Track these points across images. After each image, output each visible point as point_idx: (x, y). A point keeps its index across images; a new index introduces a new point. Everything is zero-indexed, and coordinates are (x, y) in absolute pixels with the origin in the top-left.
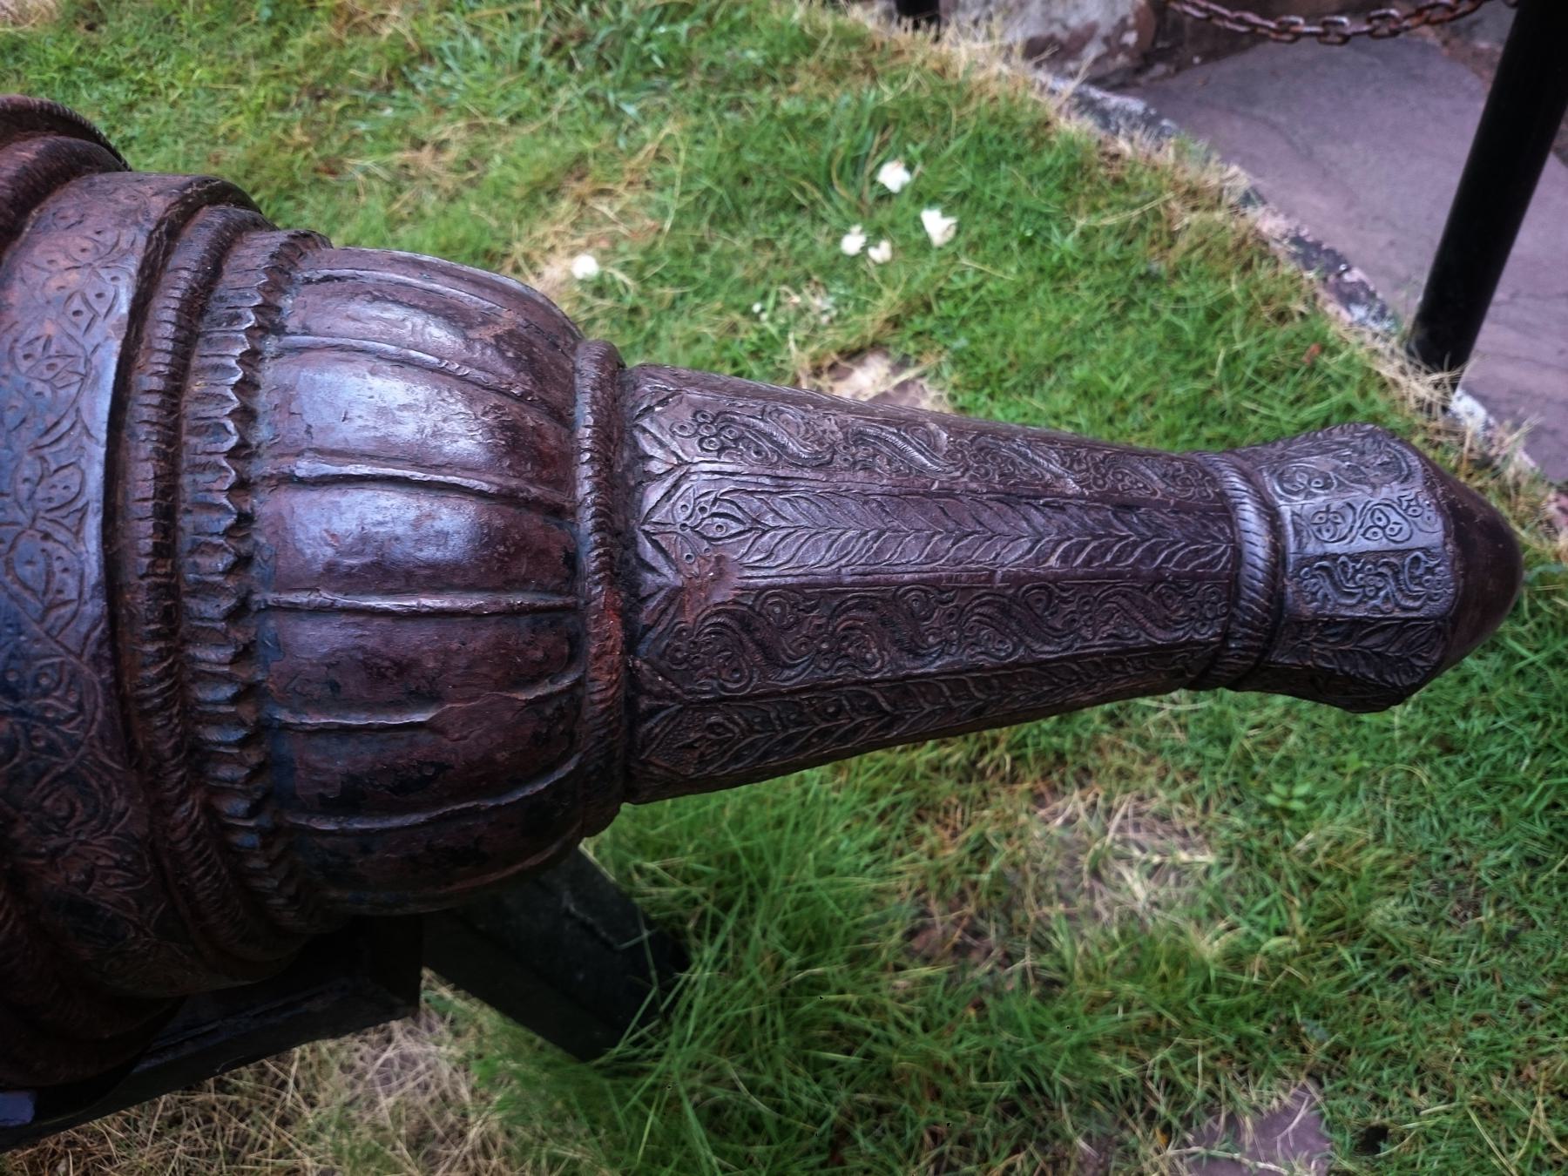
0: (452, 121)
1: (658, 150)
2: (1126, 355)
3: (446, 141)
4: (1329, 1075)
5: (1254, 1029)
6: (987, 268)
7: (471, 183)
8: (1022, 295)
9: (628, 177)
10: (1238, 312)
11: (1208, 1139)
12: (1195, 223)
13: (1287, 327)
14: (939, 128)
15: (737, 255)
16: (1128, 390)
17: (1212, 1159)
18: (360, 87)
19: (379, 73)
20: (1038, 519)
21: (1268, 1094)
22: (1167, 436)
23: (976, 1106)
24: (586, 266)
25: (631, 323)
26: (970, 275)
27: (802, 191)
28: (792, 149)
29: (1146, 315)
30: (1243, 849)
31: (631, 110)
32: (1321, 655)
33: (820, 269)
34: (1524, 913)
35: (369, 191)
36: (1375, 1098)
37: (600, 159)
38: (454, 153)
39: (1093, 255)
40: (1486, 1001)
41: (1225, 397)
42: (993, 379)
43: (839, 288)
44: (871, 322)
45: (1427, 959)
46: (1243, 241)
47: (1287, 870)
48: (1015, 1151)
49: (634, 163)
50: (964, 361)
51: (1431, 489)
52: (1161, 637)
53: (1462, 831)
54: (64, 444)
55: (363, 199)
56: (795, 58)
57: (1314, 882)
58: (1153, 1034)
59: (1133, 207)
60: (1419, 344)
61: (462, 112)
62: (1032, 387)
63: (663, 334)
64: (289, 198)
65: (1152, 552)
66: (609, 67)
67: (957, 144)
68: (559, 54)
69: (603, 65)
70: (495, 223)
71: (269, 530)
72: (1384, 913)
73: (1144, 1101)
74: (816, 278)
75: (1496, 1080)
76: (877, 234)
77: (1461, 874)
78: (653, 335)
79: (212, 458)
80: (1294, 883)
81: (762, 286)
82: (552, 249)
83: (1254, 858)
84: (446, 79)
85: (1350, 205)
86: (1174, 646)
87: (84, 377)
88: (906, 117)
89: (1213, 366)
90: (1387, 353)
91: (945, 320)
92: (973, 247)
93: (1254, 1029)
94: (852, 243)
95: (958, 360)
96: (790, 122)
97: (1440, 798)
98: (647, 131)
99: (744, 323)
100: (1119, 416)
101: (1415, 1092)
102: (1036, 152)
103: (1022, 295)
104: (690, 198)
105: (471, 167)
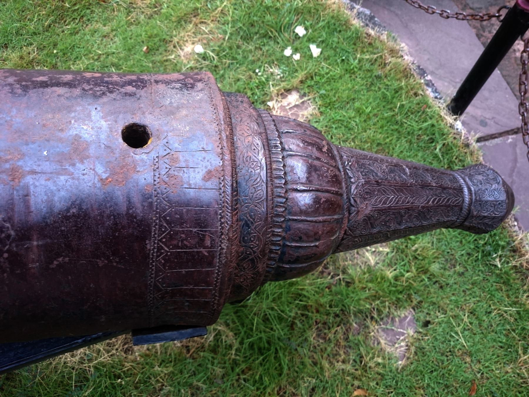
1: (222, 10)
2: (370, 101)
4: (417, 308)
5: (400, 296)
6: (330, 67)
8: (341, 77)
9: (212, 18)
10: (403, 91)
11: (386, 324)
12: (394, 62)
13: (417, 98)
14: (316, 17)
15: (251, 51)
16: (370, 112)
17: (387, 329)
20: (427, 192)
21: (403, 313)
22: (381, 128)
23: (328, 314)
24: (199, 49)
25: (215, 71)
26: (325, 69)
27: (271, 32)
28: (268, 17)
29: (377, 89)
30: (397, 248)
32: (475, 223)
33: (277, 60)
34: (465, 267)
35: (119, 11)
36: (427, 314)
37: (202, 11)
39: (362, 66)
40: (455, 290)
41: (399, 118)
42: (331, 104)
44: (295, 81)
45: (442, 279)
46: (406, 69)
47: (410, 255)
48: (338, 326)
49: (214, 14)
50: (323, 97)
51: (504, 186)
52: (446, 219)
53: (453, 246)
54: (259, 184)
55: (116, 13)
57: (416, 258)
58: (376, 297)
59: (375, 54)
60: (452, 107)
62: (342, 108)
63: (226, 76)
65: (448, 200)
70: (166, 29)
72: (435, 268)
73: (370, 314)
74: (276, 62)
75: (456, 309)
77: (452, 257)
78: (223, 76)
80: (411, 258)
81: (260, 64)
82: (187, 41)
83: (400, 251)
85: (418, 45)
86: (448, 221)
87: (260, 167)
88: (305, 11)
89: (396, 107)
90: (442, 108)
91: (317, 83)
92: (326, 59)
93: (400, 296)
94: (288, 52)
95: (322, 97)
97: (448, 237)
99: (253, 75)
100: (368, 120)
101: (437, 312)
102: (346, 31)
103: (341, 77)
104: (234, 29)
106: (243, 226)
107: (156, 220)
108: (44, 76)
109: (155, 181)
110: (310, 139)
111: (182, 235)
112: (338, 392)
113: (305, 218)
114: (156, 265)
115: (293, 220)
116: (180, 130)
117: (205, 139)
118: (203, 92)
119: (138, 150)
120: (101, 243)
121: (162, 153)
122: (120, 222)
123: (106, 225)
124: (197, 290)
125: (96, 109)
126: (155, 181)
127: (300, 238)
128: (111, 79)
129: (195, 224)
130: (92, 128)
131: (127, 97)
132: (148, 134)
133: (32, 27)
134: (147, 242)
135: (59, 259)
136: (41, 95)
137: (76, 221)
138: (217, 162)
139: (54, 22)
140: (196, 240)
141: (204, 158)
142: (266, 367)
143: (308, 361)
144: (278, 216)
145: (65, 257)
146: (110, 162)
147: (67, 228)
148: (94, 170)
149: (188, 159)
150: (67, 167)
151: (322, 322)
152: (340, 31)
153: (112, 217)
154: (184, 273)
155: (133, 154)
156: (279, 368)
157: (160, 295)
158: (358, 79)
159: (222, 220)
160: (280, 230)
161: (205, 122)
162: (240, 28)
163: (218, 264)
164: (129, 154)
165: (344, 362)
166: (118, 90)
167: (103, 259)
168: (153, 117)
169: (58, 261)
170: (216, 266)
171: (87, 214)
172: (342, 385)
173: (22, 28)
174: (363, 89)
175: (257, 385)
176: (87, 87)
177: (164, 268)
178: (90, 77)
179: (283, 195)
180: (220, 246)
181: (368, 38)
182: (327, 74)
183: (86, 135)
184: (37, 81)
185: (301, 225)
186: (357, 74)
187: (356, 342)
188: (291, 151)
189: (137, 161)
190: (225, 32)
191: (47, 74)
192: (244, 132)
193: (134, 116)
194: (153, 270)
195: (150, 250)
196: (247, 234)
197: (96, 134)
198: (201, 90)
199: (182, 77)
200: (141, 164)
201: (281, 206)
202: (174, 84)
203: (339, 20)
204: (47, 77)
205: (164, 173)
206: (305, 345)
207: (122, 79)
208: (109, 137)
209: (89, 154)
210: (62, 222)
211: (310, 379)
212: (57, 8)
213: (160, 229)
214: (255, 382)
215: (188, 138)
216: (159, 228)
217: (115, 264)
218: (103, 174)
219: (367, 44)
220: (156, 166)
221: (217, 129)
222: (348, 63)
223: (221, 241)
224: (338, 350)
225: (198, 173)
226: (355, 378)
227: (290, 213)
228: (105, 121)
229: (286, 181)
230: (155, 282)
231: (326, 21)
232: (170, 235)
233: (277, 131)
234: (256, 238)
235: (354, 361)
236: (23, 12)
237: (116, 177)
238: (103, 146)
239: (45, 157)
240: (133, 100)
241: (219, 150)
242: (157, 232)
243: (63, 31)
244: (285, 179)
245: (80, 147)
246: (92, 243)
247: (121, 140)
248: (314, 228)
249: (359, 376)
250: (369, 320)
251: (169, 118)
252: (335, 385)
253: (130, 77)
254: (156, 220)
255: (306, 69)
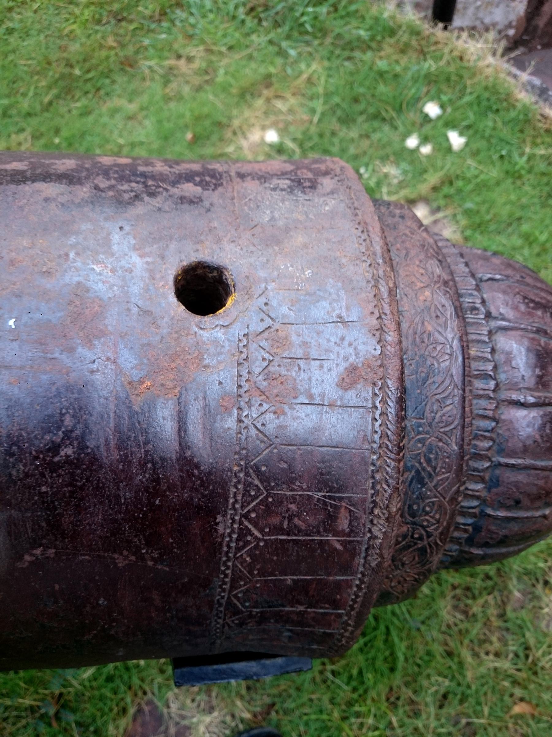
0: (197, 46)
3: (194, 57)
7: (207, 82)
8: (498, 184)
14: (458, 88)
18: (144, 18)
19: (154, 12)
24: (272, 136)
26: (472, 169)
31: (293, 52)
33: (395, 154)
35: (152, 79)
38: (197, 64)
43: (404, 165)
44: (424, 188)
48: (489, 594)
56: (384, 38)
61: (203, 42)
64: (107, 77)
66: (279, 26)
67: (467, 99)
68: (254, 14)
69: (277, 24)
71: (505, 428)
76: (425, 140)
79: (486, 392)
84: (192, 20)
91: (459, 191)
94: (412, 142)
95: (468, 213)
96: (381, 74)
98: (303, 66)
102: (508, 110)
105: (206, 72)
106: (411, 482)
107: (239, 471)
108: (21, 161)
109: (239, 386)
110: (537, 295)
111: (290, 506)
112: (486, 704)
113: (532, 462)
114: (234, 566)
115: (507, 465)
116: (292, 277)
117: (344, 297)
118: (335, 196)
119: (208, 319)
120: (123, 519)
121: (256, 326)
122: (166, 477)
123: (137, 481)
124: (313, 615)
125: (121, 228)
126: (239, 386)
127: (518, 502)
128: (150, 169)
129: (319, 482)
130: (113, 271)
131: (186, 206)
132: (228, 285)
133: (25, 105)
134: (219, 518)
135: (35, 552)
136: (10, 198)
137: (72, 475)
138: (370, 348)
139: (58, 97)
140: (320, 517)
141: (343, 339)
142: (370, 656)
143: (437, 649)
144: (477, 456)
145: (47, 547)
146: (149, 345)
147: (52, 488)
148: (114, 362)
149: (308, 340)
150: (57, 355)
151: (463, 586)
152: (497, 111)
153: (150, 465)
154: (289, 582)
155: (196, 329)
156: (390, 659)
157: (237, 619)
158: (527, 188)
159: (378, 476)
160: (479, 486)
161: (344, 261)
162: (338, 105)
163: (361, 569)
164: (189, 329)
165: (497, 655)
166: (166, 190)
167: (125, 553)
168: (238, 249)
169: (32, 555)
170: (357, 573)
171: (97, 460)
172: (493, 692)
173: (10, 106)
174: (534, 204)
175: (354, 683)
176: (103, 183)
177: (251, 572)
178: (109, 163)
179: (490, 413)
180: (370, 531)
181: (544, 121)
182: (476, 177)
183: (100, 285)
184: (6, 170)
185: (521, 477)
186: (525, 179)
187: (519, 622)
188: (504, 319)
189: (204, 343)
190: (313, 111)
191: (26, 158)
192: (414, 279)
193: (199, 247)
194: (226, 576)
195: (223, 535)
196: (417, 498)
197: (120, 283)
198: (332, 192)
199: (289, 167)
200: (212, 350)
201: (485, 437)
202: (275, 181)
203: (498, 93)
204: (26, 163)
205: (258, 370)
206: (433, 622)
207: (173, 170)
208: (147, 290)
209: (106, 326)
210: (43, 475)
211: (440, 679)
212: (63, 77)
213: (246, 492)
214: (350, 677)
215: (308, 294)
216: (245, 490)
217: (150, 563)
218: (135, 372)
219: (542, 131)
220: (244, 356)
221: (369, 276)
222: (510, 162)
223: (372, 522)
224: (487, 632)
225: (330, 370)
226: (515, 683)
227: (501, 452)
228: (141, 256)
229: (497, 385)
230: (229, 598)
231: (475, 95)
232: (267, 506)
233: (473, 275)
234: (436, 507)
235: (517, 655)
236: (14, 82)
237: (160, 379)
238: (135, 310)
239: (11, 330)
240: (197, 212)
241: (375, 322)
242: (239, 497)
243: (69, 111)
244: (495, 379)
245: (87, 311)
246: (104, 520)
247: (172, 298)
248: (546, 483)
249: (524, 680)
250: (540, 586)
251: (270, 251)
252: (481, 693)
253: (188, 166)
254: (239, 471)
255: (442, 168)
